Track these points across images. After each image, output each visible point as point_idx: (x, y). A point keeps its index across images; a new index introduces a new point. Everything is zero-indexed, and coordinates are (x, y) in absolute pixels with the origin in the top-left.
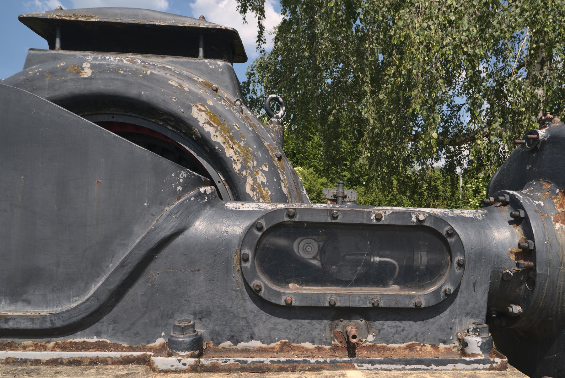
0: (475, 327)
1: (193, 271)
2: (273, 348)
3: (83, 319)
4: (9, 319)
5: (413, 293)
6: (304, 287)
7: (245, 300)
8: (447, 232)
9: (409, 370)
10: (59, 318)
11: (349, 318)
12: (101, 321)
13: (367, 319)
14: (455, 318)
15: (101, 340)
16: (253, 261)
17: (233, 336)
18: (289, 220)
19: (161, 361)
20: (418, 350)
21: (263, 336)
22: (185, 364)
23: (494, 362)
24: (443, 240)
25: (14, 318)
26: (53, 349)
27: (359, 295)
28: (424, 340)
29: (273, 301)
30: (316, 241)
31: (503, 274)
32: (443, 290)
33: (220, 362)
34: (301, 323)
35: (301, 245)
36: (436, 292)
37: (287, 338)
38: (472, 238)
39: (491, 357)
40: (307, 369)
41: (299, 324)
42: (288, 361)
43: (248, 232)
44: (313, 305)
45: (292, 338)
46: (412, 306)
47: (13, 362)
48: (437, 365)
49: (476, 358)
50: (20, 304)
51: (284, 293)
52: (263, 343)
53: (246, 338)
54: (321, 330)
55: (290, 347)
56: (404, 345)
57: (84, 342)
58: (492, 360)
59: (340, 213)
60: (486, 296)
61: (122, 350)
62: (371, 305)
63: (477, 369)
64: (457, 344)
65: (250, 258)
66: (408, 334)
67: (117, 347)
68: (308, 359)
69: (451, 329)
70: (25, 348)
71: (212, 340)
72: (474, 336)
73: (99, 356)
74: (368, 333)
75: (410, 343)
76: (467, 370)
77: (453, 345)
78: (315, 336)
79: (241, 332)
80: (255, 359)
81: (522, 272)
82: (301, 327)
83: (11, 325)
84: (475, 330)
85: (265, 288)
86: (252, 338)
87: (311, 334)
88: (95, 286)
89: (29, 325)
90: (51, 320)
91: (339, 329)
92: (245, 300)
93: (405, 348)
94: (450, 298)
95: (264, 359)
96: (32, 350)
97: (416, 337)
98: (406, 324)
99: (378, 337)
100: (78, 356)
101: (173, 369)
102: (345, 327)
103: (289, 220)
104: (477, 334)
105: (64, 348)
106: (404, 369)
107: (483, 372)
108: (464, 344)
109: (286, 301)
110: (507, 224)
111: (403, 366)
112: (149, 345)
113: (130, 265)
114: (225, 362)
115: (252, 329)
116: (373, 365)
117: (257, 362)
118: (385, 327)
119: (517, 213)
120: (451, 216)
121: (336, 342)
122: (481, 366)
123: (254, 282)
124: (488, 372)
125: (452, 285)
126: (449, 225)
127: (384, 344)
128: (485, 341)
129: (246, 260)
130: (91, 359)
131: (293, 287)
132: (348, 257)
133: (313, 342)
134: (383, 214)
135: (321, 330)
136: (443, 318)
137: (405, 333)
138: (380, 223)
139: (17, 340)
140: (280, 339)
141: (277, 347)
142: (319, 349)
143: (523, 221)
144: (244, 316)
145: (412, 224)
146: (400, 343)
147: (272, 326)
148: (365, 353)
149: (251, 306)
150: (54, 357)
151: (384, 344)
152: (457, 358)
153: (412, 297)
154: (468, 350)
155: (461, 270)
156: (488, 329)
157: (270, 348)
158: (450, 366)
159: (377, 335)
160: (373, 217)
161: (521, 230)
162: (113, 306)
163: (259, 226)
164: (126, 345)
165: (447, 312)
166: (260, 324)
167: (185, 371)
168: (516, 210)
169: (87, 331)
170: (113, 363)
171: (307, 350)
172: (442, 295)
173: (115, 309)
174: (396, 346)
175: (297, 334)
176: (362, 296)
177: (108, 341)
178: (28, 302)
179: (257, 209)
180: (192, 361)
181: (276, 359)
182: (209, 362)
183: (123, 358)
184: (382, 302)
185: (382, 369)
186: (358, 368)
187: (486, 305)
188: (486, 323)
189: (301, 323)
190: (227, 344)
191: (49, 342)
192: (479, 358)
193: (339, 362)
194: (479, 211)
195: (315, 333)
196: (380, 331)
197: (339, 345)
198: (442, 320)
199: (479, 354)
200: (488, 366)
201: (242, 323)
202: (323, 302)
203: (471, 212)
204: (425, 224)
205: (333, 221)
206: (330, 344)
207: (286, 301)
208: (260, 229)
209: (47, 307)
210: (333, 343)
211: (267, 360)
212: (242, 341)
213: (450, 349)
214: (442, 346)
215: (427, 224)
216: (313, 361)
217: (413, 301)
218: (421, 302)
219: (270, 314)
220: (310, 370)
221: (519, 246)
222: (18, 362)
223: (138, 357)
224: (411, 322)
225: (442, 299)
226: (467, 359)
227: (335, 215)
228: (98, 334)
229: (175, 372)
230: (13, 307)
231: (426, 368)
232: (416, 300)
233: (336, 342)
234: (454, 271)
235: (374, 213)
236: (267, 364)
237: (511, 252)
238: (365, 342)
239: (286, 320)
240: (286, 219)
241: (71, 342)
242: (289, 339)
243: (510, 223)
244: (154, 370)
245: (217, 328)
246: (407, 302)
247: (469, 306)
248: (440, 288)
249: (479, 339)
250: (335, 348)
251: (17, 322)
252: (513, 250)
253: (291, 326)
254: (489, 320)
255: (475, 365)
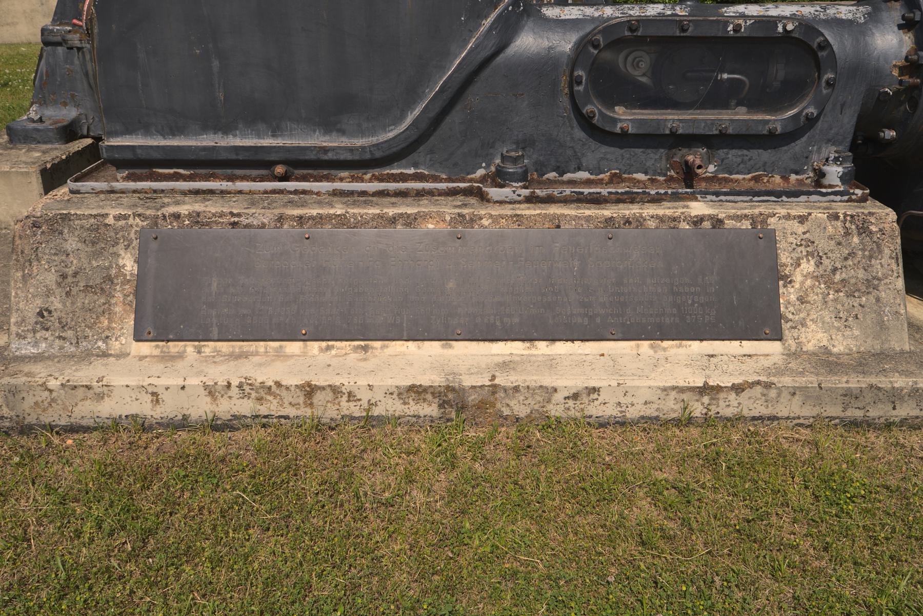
0: (837, 155)
1: (516, 96)
2: (602, 179)
3: (403, 149)
4: (328, 150)
5: (768, 117)
6: (633, 111)
7: (572, 128)
8: (819, 44)
9: (757, 202)
10: (379, 149)
11: (689, 147)
12: (418, 151)
13: (709, 147)
14: (814, 146)
15: (419, 171)
16: (586, 84)
17: (559, 167)
18: (630, 34)
19: (494, 193)
20: (765, 181)
21: (591, 167)
22: (519, 195)
23: (853, 194)
24: (813, 53)
25: (333, 149)
26: (370, 181)
27: (705, 121)
28: (773, 170)
29: (607, 129)
30: (648, 53)
31: (880, 94)
32: (804, 114)
33: (555, 193)
34: (634, 152)
35: (630, 59)
36: (796, 117)
37: (617, 169)
38: (847, 49)
39: (851, 188)
40: (646, 200)
41: (632, 154)
42: (626, 193)
43: (581, 46)
44: (651, 133)
45: (624, 168)
46: (765, 132)
47: (340, 193)
48: (788, 197)
49: (833, 190)
50: (334, 133)
51: (620, 119)
52: (591, 174)
53: (572, 169)
54: (656, 160)
55: (621, 178)
56: (749, 176)
57: (401, 173)
58: (852, 191)
59: (691, 24)
60: (855, 119)
61: (441, 181)
62: (717, 132)
63: (833, 201)
64: (811, 175)
65: (584, 81)
66: (755, 164)
67: (436, 179)
68: (647, 190)
69: (807, 157)
70: (341, 180)
71: (536, 171)
72: (835, 166)
73: (426, 188)
74: (710, 164)
75: (757, 173)
76: (821, 202)
77: (807, 176)
78: (649, 167)
79: (567, 162)
80: (592, 190)
81: (904, 90)
82: (634, 156)
83: (330, 156)
84: (836, 159)
85: (599, 114)
86: (579, 169)
87: (645, 165)
88: (411, 113)
89: (349, 156)
90: (370, 151)
91: (677, 159)
92: (572, 128)
93: (750, 180)
94: (811, 122)
95: (602, 190)
96: (349, 182)
97: (764, 167)
98: (754, 153)
99: (721, 168)
100: (404, 187)
101: (507, 200)
102: (683, 156)
103: (630, 34)
104: (839, 163)
105: (381, 179)
106: (751, 201)
107: (840, 204)
108: (821, 174)
109: (622, 128)
110: (896, 28)
111: (751, 197)
112: (469, 177)
113: (450, 90)
114: (561, 193)
115: (579, 159)
116: (717, 196)
117: (594, 193)
118: (730, 156)
119: (912, 15)
120: (824, 18)
121: (672, 173)
122: (838, 198)
123: (586, 108)
124: (845, 204)
125: (815, 108)
126: (823, 35)
127: (727, 175)
128: (846, 171)
129: (579, 83)
130: (416, 190)
131: (620, 111)
132: (689, 74)
133: (646, 173)
134: (743, 24)
135: (656, 160)
136: (798, 146)
137: (752, 162)
138: (738, 35)
139: (333, 172)
140: (609, 170)
141: (607, 179)
142: (652, 181)
143: (918, 26)
144: (571, 145)
145: (777, 35)
146: (745, 174)
147: (602, 156)
148: (704, 184)
149: (579, 134)
150: (381, 189)
151: (727, 175)
152: (811, 190)
153: (767, 122)
154: (826, 181)
155: (830, 90)
156: (851, 158)
157: (599, 179)
158: (803, 198)
159: (719, 166)
160: (730, 28)
161: (912, 37)
162: (430, 136)
163: (596, 43)
164: (444, 177)
165: (804, 139)
166: (588, 154)
167: (520, 202)
168: (911, 11)
169: (404, 161)
170: (440, 195)
171: (639, 181)
172: (802, 119)
173: (432, 138)
174: (740, 177)
175: (629, 165)
176: (708, 122)
177: (426, 173)
178: (342, 132)
179: (581, 17)
180: (526, 192)
181: (613, 190)
182: (544, 193)
183: (449, 189)
184: (731, 128)
185: (727, 201)
186: (701, 199)
187: (853, 131)
188: (850, 151)
189: (634, 152)
190: (552, 175)
191: (365, 174)
192: (837, 189)
193: (681, 193)
194: (861, 8)
195: (649, 163)
196: (722, 160)
197: (675, 176)
198: (797, 149)
199: (837, 186)
200: (846, 198)
201: (569, 152)
202: (664, 129)
203: (850, 12)
204: (793, 35)
205: (682, 35)
206: (665, 175)
207: (622, 128)
208: (596, 47)
209: (362, 137)
210: (669, 174)
211: (604, 191)
212: (569, 172)
213: (802, 180)
214: (793, 177)
215: (796, 35)
216: (653, 192)
217: (767, 127)
218: (776, 128)
219: (600, 142)
220: (649, 202)
221: (906, 59)
222: (344, 193)
223: (465, 188)
224: (760, 151)
225: (802, 124)
226: (824, 190)
227: (685, 28)
228: (416, 165)
229: (510, 203)
230: (327, 138)
231: (776, 199)
232: (771, 126)
233: (672, 173)
234: (821, 91)
235: (732, 23)
236: (604, 196)
237: (895, 66)
238: (705, 172)
239: (618, 149)
240: (627, 33)
241: (388, 173)
242: (620, 170)
243: (900, 27)
244: (488, 201)
245: (541, 158)
246: (760, 128)
247: (833, 132)
248: (802, 111)
249: (840, 169)
250: (670, 179)
251: (337, 153)
252: (898, 64)
253: (622, 156)
254: (853, 147)
255: (832, 197)
